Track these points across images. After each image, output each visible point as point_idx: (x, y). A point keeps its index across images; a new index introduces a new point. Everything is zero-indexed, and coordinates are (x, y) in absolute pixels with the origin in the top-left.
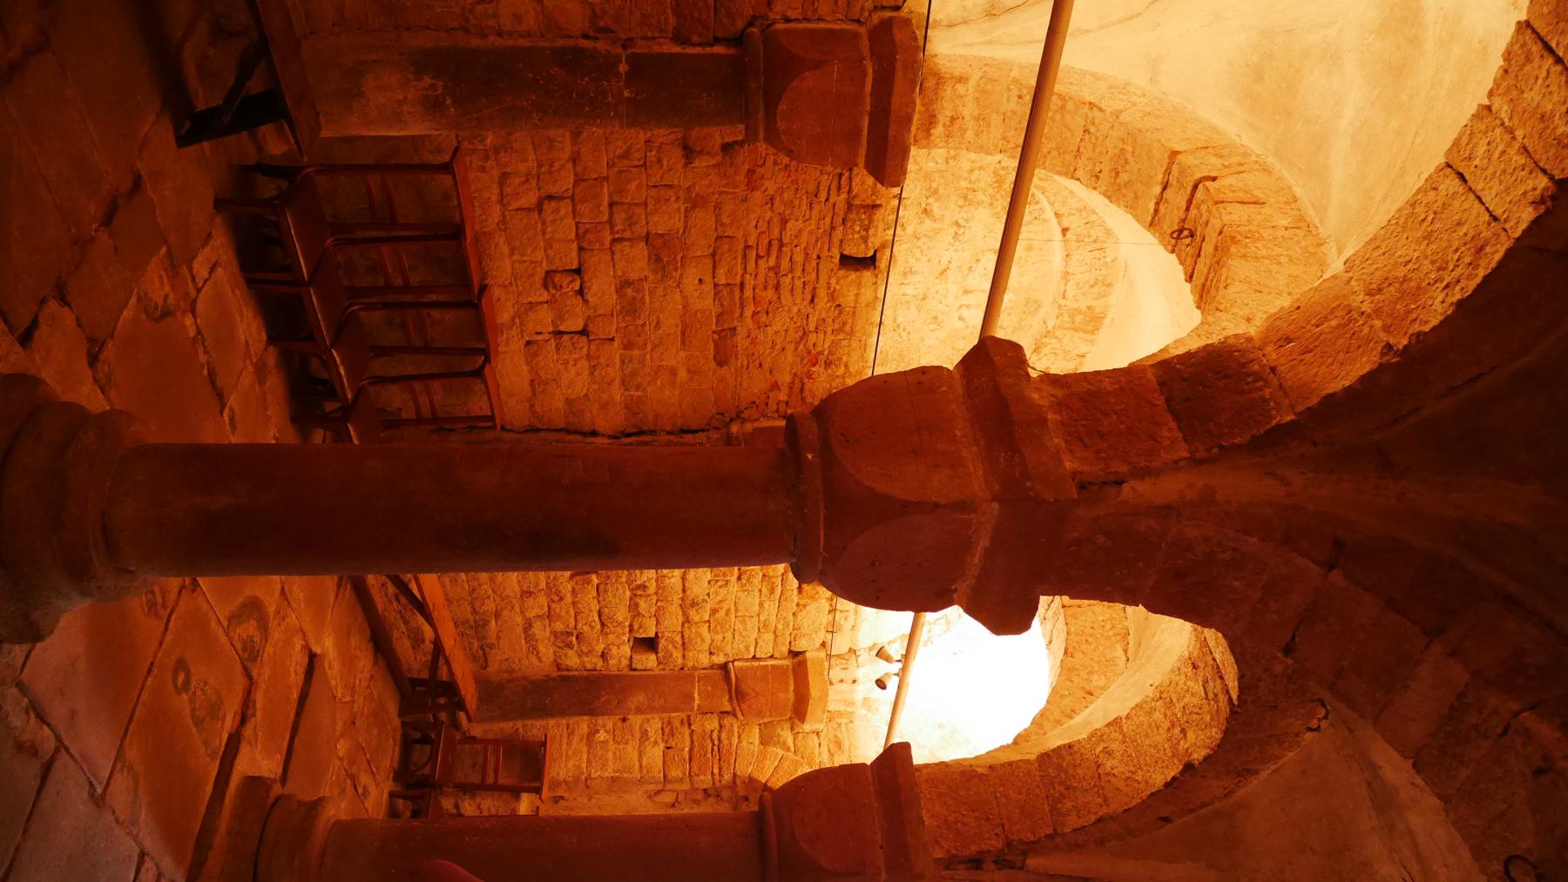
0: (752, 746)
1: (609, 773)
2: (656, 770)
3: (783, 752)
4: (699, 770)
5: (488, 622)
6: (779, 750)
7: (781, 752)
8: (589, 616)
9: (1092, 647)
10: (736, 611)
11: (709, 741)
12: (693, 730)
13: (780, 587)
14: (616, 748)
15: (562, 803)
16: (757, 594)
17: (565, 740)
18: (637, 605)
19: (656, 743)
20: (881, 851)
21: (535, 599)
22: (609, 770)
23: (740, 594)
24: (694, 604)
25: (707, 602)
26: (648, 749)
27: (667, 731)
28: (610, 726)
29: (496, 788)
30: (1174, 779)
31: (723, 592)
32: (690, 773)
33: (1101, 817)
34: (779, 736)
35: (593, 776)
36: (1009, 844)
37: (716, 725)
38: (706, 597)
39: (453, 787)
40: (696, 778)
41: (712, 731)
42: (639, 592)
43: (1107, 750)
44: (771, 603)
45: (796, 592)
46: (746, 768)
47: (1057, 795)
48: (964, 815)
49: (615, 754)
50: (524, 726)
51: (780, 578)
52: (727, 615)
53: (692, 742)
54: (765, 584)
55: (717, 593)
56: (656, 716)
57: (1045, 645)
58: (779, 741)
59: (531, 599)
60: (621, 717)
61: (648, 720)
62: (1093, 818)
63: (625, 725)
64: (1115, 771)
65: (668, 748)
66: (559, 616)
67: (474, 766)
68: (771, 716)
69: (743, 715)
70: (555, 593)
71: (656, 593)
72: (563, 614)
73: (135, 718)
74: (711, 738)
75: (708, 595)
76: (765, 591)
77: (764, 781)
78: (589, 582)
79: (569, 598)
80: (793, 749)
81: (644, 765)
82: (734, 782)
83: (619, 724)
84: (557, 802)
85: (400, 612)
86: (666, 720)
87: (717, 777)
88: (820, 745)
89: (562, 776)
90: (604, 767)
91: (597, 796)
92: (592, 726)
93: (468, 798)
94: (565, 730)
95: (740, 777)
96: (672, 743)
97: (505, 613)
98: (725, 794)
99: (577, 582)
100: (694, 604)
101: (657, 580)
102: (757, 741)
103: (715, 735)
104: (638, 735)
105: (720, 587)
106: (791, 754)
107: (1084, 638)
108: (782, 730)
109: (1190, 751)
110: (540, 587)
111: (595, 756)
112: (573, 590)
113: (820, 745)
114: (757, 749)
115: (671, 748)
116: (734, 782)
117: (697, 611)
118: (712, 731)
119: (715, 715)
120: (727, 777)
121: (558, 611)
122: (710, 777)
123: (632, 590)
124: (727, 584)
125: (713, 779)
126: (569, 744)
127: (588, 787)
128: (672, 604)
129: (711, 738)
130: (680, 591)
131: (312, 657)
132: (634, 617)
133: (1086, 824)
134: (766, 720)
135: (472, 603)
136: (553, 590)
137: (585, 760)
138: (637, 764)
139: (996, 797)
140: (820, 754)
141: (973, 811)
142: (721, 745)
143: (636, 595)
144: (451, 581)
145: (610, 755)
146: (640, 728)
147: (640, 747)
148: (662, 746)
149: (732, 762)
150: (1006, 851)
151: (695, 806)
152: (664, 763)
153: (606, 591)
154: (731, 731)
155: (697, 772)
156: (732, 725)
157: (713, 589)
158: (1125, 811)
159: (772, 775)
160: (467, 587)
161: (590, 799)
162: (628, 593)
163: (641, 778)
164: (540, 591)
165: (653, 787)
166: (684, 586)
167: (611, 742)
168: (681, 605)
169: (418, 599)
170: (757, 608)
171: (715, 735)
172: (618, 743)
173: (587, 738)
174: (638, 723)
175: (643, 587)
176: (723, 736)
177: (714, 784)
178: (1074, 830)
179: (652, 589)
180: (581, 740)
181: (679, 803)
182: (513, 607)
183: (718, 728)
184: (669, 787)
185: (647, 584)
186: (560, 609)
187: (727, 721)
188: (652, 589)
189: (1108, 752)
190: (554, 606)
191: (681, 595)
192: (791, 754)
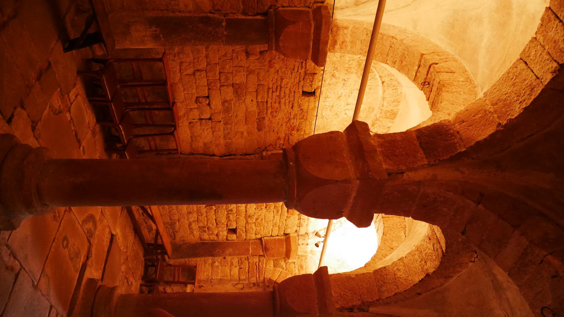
0: (271, 268)
1: (219, 277)
2: (236, 276)
3: (281, 270)
5: (176, 223)
6: (280, 269)
10: (265, 219)
12: (249, 262)
13: (280, 210)
14: (222, 268)
17: (203, 265)
18: (229, 217)
19: (236, 266)
24: (250, 216)
25: (254, 216)
27: (240, 262)
28: (219, 260)
29: (179, 283)
30: (422, 279)
31: (260, 212)
32: (248, 277)
33: (396, 293)
34: (280, 264)
35: (213, 278)
36: (363, 303)
37: (257, 260)
38: (254, 214)
41: (256, 262)
42: (230, 212)
45: (286, 212)
46: (268, 275)
48: (347, 292)
49: (221, 270)
50: (189, 260)
53: (249, 266)
54: (275, 209)
58: (280, 266)
62: (393, 293)
64: (401, 277)
65: (240, 268)
68: (277, 257)
69: (267, 256)
70: (200, 213)
71: (236, 213)
74: (256, 265)
75: (255, 213)
77: (275, 280)
79: (205, 214)
81: (232, 274)
82: (264, 281)
84: (200, 288)
86: (240, 258)
87: (258, 279)
88: (295, 267)
90: (217, 275)
91: (215, 285)
92: (213, 260)
94: (203, 262)
95: (266, 279)
96: (242, 266)
97: (182, 220)
98: (261, 285)
99: (207, 209)
100: (250, 216)
101: (236, 208)
102: (272, 266)
103: (257, 263)
104: (229, 264)
105: (259, 210)
106: (284, 271)
108: (281, 262)
110: (195, 210)
112: (206, 211)
113: (295, 267)
114: (272, 269)
116: (264, 281)
118: (256, 262)
119: (257, 256)
120: (262, 278)
121: (201, 219)
122: (255, 279)
124: (261, 209)
125: (257, 279)
126: (205, 267)
128: (242, 217)
131: (112, 236)
135: (170, 216)
136: (199, 212)
137: (210, 272)
138: (229, 274)
141: (350, 291)
143: (229, 213)
145: (220, 271)
148: (238, 268)
149: (264, 273)
150: (362, 305)
152: (239, 274)
153: (218, 212)
156: (263, 260)
157: (256, 211)
158: (405, 291)
159: (278, 278)
160: (168, 211)
161: (212, 287)
162: (226, 213)
165: (235, 282)
166: (246, 210)
167: (220, 266)
169: (150, 214)
170: (272, 218)
171: (257, 263)
173: (211, 265)
174: (230, 259)
176: (260, 264)
180: (209, 265)
181: (244, 288)
182: (184, 218)
183: (258, 261)
184: (240, 282)
186: (202, 218)
187: (262, 259)
190: (199, 217)
191: (245, 213)
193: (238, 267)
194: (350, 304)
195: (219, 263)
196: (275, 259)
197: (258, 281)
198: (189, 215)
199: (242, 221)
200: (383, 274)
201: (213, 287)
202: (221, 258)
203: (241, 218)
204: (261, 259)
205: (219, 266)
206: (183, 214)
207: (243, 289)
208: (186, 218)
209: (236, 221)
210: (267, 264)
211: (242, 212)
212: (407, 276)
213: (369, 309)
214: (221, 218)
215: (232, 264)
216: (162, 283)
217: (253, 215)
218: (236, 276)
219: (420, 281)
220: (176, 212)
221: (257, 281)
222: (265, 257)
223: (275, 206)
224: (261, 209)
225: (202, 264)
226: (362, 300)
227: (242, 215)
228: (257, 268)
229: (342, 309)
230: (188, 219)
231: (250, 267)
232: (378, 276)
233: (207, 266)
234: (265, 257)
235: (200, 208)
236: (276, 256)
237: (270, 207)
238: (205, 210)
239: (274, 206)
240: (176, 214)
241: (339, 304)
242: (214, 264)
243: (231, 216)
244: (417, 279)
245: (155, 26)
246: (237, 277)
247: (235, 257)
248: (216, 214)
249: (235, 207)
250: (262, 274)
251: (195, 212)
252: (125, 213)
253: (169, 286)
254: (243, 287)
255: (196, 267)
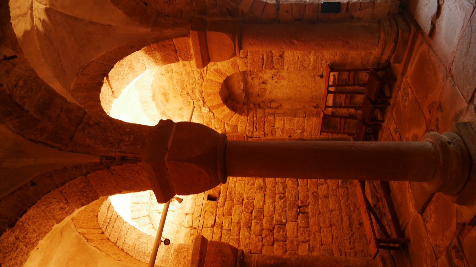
0: (241, 125)
1: (296, 119)
2: (278, 119)
3: (229, 123)
4: (261, 119)
5: (342, 183)
6: (231, 124)
7: (230, 123)
8: (302, 184)
9: (86, 217)
10: (245, 183)
11: (258, 128)
12: (264, 132)
13: (227, 195)
14: (293, 127)
15: (315, 105)
16: (236, 192)
17: (313, 131)
18: (283, 189)
19: (278, 128)
20: (168, 168)
21: (323, 194)
22: (296, 120)
23: (243, 192)
24: (261, 188)
25: (256, 189)
26: (281, 126)
27: (274, 132)
28: (295, 135)
29: (341, 117)
30: (21, 216)
31: (249, 194)
32: (265, 118)
33: (62, 186)
34: (230, 129)
35: (303, 118)
36: (108, 168)
37: (255, 133)
38: (256, 191)
39: (358, 118)
40: (263, 115)
41: (256, 131)
42: (282, 195)
43: (63, 209)
44: (231, 186)
45: (221, 192)
46: (243, 119)
47: (86, 188)
48: (131, 176)
49: (294, 125)
50: (329, 136)
51: (227, 199)
52: (248, 182)
53: (264, 128)
54: (233, 197)
55: (252, 194)
56: (277, 137)
57: (112, 204)
58: (231, 127)
59: (325, 194)
60: (291, 138)
61: (281, 136)
62: (66, 184)
63: (290, 135)
64: (57, 204)
65: (273, 126)
66: (314, 184)
67: (349, 123)
68: (233, 136)
69: (244, 137)
70: (315, 197)
71: (276, 194)
72: (312, 185)
73: (464, 99)
74: (256, 129)
75: (255, 193)
76: (233, 193)
77: (236, 114)
78: (302, 202)
79: (310, 193)
80: (225, 124)
81: (283, 121)
82: (248, 112)
83: (292, 135)
84: (317, 105)
85: (377, 192)
86: (274, 135)
87: (255, 115)
88: (215, 125)
89: (315, 119)
90: (298, 121)
91: (301, 107)
92: (303, 135)
93: (352, 113)
94: (313, 134)
95: (246, 115)
96: (272, 128)
97: (335, 187)
98: (252, 105)
99: (306, 202)
100: (261, 188)
101: (275, 201)
102: (239, 127)
103: (255, 130)
104: (285, 131)
105: (250, 196)
106: (226, 122)
107: (90, 220)
108: (229, 131)
109: (12, 233)
110: (321, 200)
111: (302, 125)
112: (308, 198)
113: (215, 125)
114: (239, 124)
115: (272, 126)
116: (248, 112)
117: (260, 185)
118: (256, 131)
119: (255, 137)
120: (250, 115)
121: (314, 188)
122: (257, 116)
123: (285, 196)
124: (248, 198)
125: (256, 114)
126: (311, 129)
127: (305, 113)
128: (270, 189)
129: (256, 129)
130: (266, 195)
131: (422, 212)
132: (285, 182)
133: (70, 182)
134: (236, 134)
135: (348, 193)
136: (316, 198)
137: (305, 124)
138: (285, 121)
139: (117, 183)
140: (215, 122)
141: (127, 178)
142: (253, 126)
143: (284, 194)
144: (356, 205)
145: (296, 125)
146: (284, 133)
147: (284, 127)
148: (276, 127)
149: (248, 121)
150: (110, 165)
151: (264, 100)
152: (275, 121)
153: (295, 197)
154: (249, 131)
155: (262, 118)
156: (249, 133)
157: (253, 196)
158: (50, 191)
159: (233, 116)
160: (350, 201)
161: (304, 106)
162: (287, 195)
163: (284, 117)
164: (321, 198)
165: (280, 111)
166: (265, 198)
167: (295, 129)
168: (266, 188)
169: (372, 214)
170: (237, 185)
171: (255, 130)
172: (292, 129)
173: (304, 131)
174: (284, 135)
175: (281, 198)
176: (252, 129)
177: (256, 111)
178: (76, 178)
179: (277, 196)
180: (307, 130)
181: (270, 102)
182: (332, 190)
183: (254, 132)
184: (273, 111)
185: (279, 199)
186: (313, 188)
187: (250, 134)
188: (277, 196)
189: (63, 208)
190: (316, 190)
191: (266, 193)
192: (226, 122)
193: (276, 128)
194: (125, 166)
195: (296, 132)
196: (236, 133)
197: (254, 111)
198: (327, 194)
199: (269, 182)
200: (85, 198)
201: (303, 106)
202: (293, 138)
203: (271, 187)
204: (251, 134)
205: (297, 130)
206: (334, 196)
207: (271, 101)
208: (330, 189)
209: (276, 183)
210: (245, 129)
211: (269, 195)
212: (48, 209)
213: (99, 161)
214: (293, 187)
215: (282, 131)
216: (359, 118)
217: (257, 190)
218: (278, 119)
219: (25, 212)
220: (341, 198)
221: (256, 111)
222: (247, 136)
223: (233, 201)
224: (249, 199)
225: (314, 132)
226: (110, 170)
227: (269, 191)
228: (255, 125)
229: (136, 160)
230: (328, 187)
231: (263, 128)
232: (92, 195)
233: (309, 129)
234: (247, 136)
235: (314, 203)
236: (234, 137)
237: (239, 200)
238: (309, 199)
239: (234, 202)
240: (341, 196)
241: (140, 166)
242: (302, 132)
243: (281, 189)
244: (31, 212)
245: (330, 64)
246: (277, 118)
247: (279, 136)
248: (297, 194)
249: (277, 202)
250: (250, 120)
251: (320, 197)
252: (401, 220)
253: (351, 113)
254: (271, 103)
255: (321, 131)
